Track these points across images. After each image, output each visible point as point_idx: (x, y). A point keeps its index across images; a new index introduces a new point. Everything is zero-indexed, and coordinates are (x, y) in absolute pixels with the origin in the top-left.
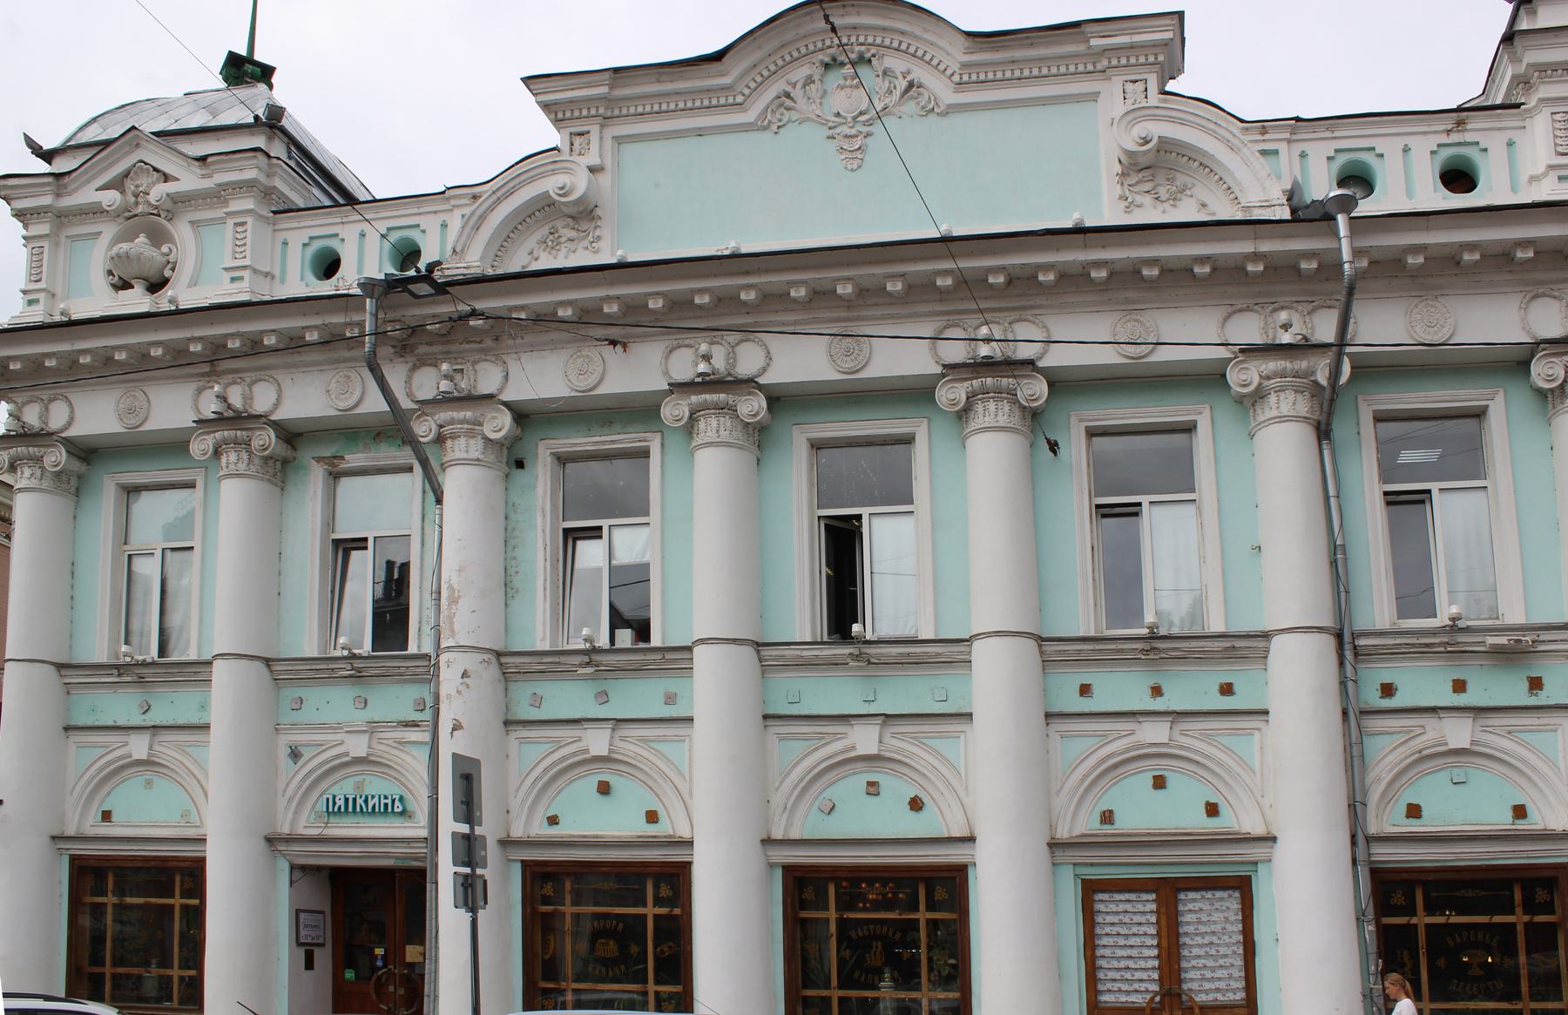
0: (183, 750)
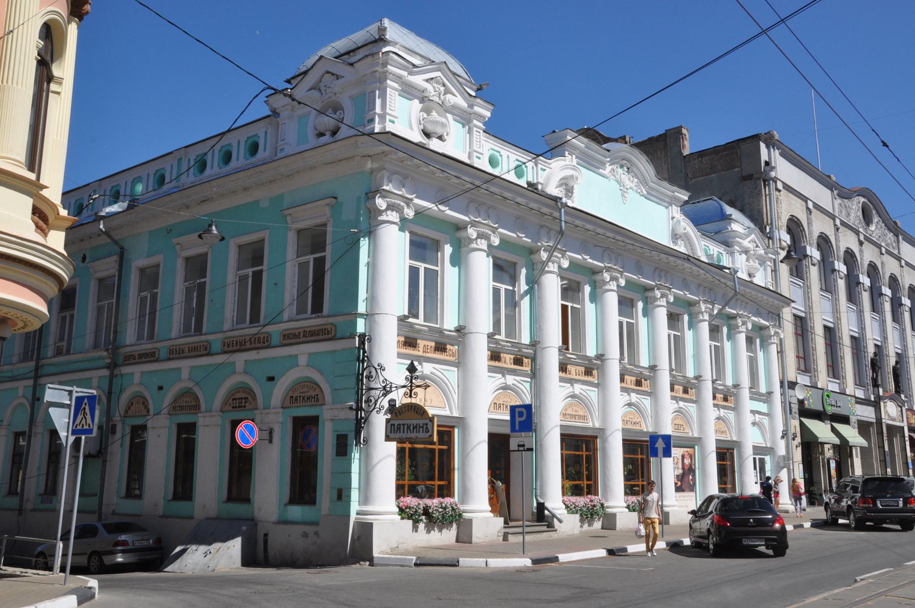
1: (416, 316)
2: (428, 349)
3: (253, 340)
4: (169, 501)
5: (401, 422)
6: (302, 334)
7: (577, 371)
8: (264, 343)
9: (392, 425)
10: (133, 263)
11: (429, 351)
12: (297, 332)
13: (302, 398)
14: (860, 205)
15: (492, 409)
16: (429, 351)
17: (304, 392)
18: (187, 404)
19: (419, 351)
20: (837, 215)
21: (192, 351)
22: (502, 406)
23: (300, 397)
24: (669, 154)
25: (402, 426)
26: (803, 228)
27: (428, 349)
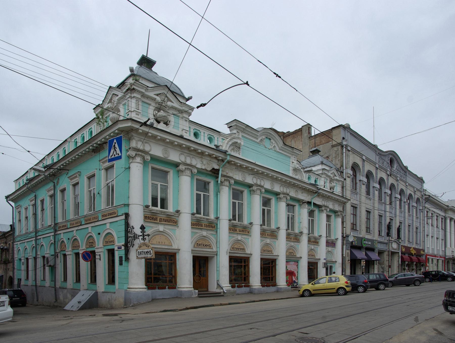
0: (174, 95)
1: (264, 225)
2: (162, 220)
4: (106, 285)
5: (141, 251)
7: (240, 230)
11: (162, 221)
14: (389, 159)
15: (196, 246)
16: (162, 221)
17: (109, 239)
20: (377, 163)
22: (201, 245)
24: (303, 137)
26: (360, 168)
27: (162, 220)
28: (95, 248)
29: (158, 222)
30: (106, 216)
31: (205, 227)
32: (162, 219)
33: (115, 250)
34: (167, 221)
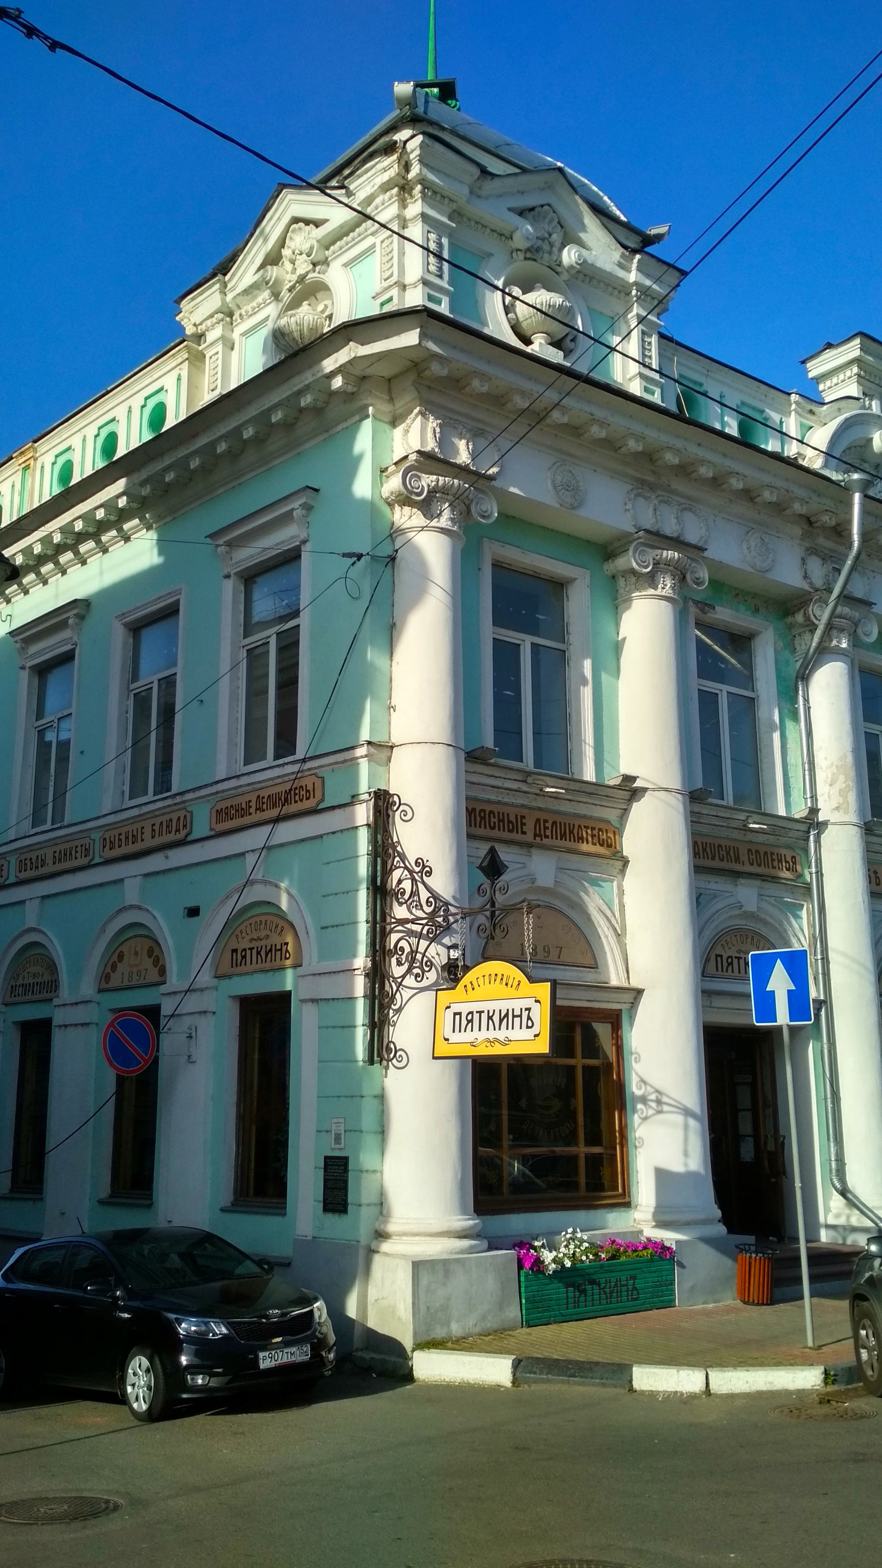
2: (546, 828)
3: (156, 828)
5: (475, 1007)
6: (253, 804)
8: (178, 830)
9: (455, 1014)
10: (588, 574)
11: (548, 833)
12: (243, 800)
13: (254, 951)
16: (548, 833)
18: (36, 980)
19: (524, 833)
21: (60, 860)
22: (735, 961)
23: (251, 949)
25: (476, 1016)
27: (546, 828)
28: (163, 989)
29: (529, 837)
30: (242, 811)
31: (752, 864)
32: (549, 825)
33: (54, 1023)
34: (571, 832)
